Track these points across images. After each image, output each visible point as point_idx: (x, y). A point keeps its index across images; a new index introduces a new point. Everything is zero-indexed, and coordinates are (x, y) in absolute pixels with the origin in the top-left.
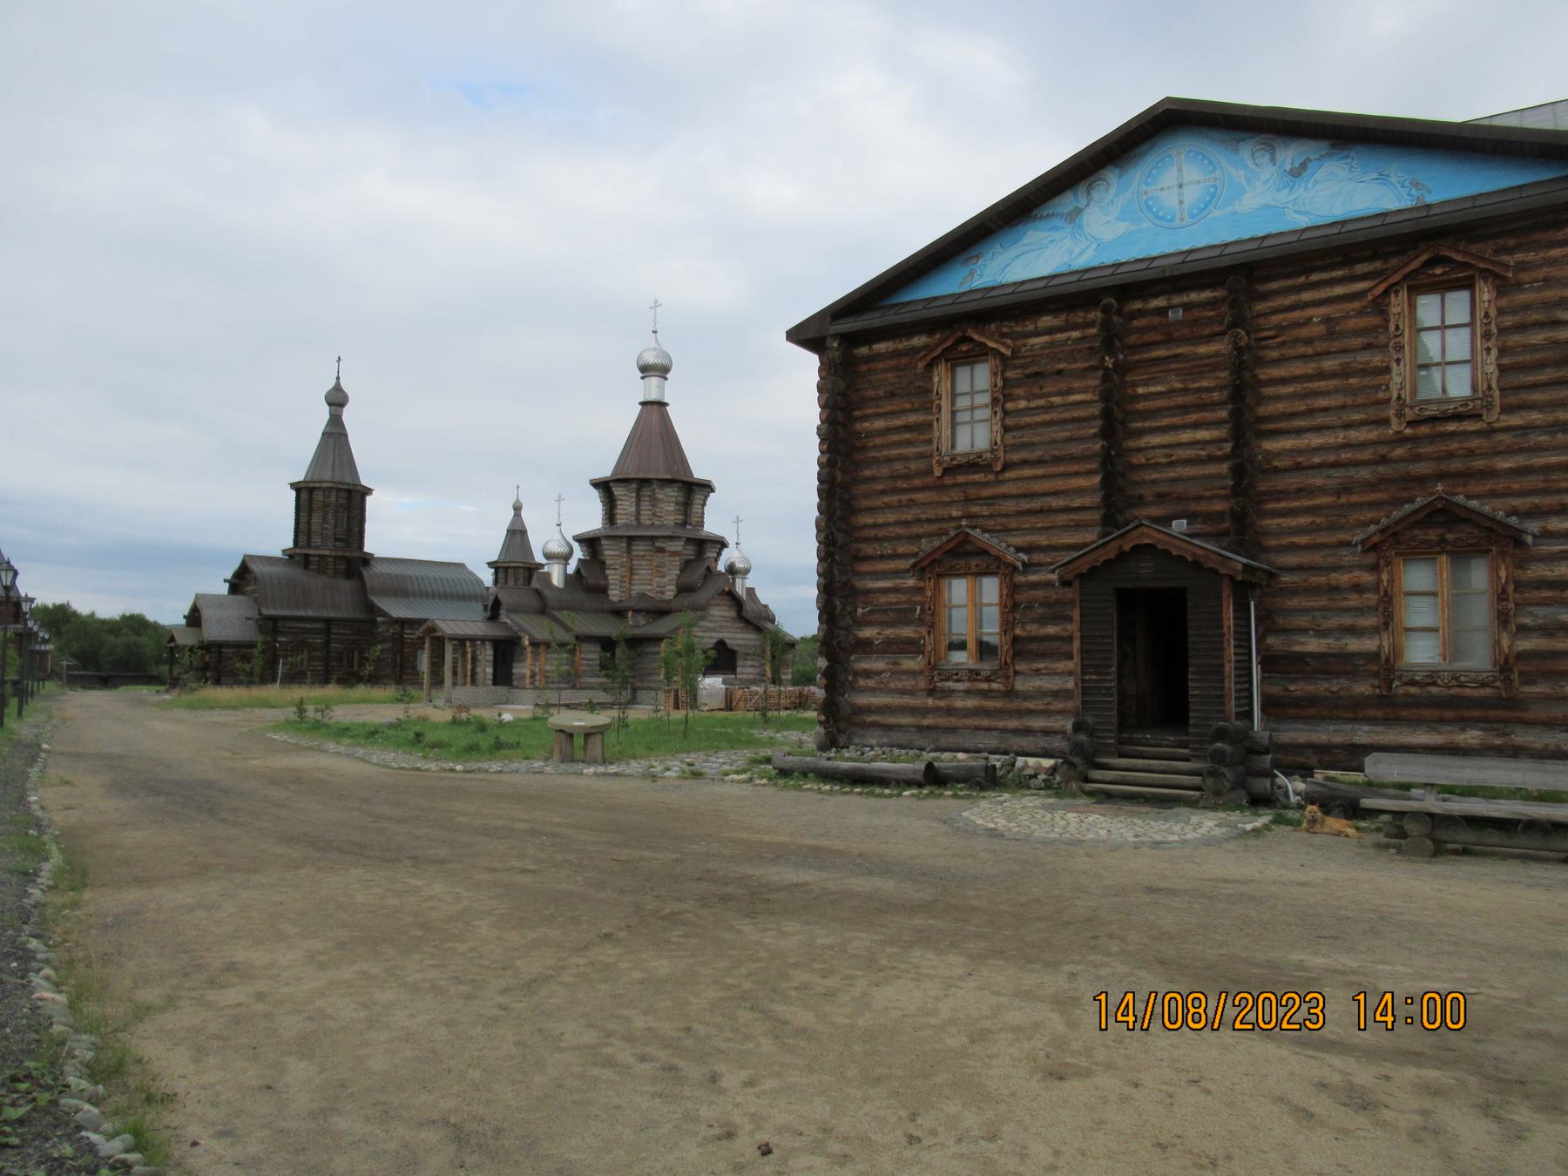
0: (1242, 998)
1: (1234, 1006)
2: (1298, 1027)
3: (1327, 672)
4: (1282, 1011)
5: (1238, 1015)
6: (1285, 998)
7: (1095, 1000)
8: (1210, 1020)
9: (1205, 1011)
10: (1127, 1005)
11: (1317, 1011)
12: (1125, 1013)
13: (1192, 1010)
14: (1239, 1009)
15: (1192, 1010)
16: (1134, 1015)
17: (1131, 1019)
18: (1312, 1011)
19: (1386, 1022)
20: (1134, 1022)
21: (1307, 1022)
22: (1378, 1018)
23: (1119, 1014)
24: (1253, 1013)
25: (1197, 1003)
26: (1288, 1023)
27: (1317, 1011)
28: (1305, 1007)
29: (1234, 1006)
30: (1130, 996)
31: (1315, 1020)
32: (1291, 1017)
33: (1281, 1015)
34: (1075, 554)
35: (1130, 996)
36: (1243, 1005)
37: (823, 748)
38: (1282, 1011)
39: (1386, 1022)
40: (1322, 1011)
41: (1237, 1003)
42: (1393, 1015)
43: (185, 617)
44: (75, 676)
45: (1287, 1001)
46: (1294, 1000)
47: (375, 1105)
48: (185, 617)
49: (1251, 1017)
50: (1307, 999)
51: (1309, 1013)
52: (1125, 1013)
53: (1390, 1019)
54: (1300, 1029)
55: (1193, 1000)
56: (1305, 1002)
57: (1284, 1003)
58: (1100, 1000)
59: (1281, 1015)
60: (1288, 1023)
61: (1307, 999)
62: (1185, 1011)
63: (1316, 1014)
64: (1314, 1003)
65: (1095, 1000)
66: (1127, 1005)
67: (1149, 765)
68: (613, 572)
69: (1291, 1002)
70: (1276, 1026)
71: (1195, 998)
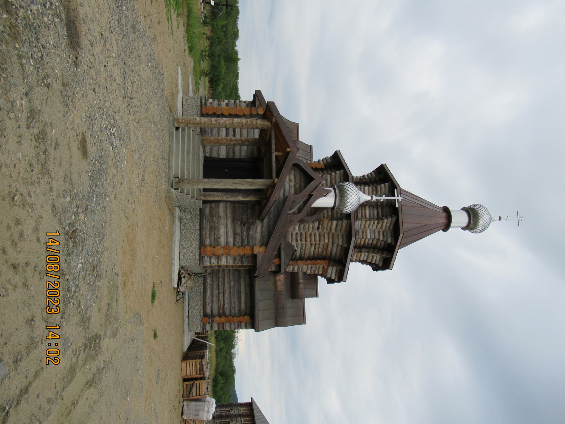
0: (57, 284)
1: (55, 281)
2: (47, 304)
3: (247, 296)
4: (53, 358)
5: (52, 283)
6: (58, 359)
7: (57, 231)
8: (49, 272)
9: (53, 313)
10: (55, 243)
11: (53, 311)
12: (52, 242)
13: (53, 269)
14: (54, 283)
15: (53, 266)
16: (51, 245)
17: (50, 244)
18: (53, 309)
19: (49, 243)
20: (49, 245)
21: (49, 308)
22: (50, 333)
23: (52, 240)
24: (53, 288)
25: (56, 268)
26: (49, 301)
27: (53, 311)
28: (54, 307)
29: (55, 281)
30: (58, 243)
31: (49, 310)
32: (50, 284)
33: (51, 357)
34: (417, 206)
35: (58, 243)
36: (55, 284)
37: (292, 181)
38: (53, 358)
39: (49, 243)
40: (53, 313)
41: (56, 282)
42: (51, 338)
43: (258, 95)
44: (195, 171)
45: (57, 309)
46: (57, 286)
47: (31, 165)
48: (258, 95)
49: (50, 287)
50: (57, 308)
51: (52, 308)
52: (52, 335)
53: (50, 337)
54: (46, 305)
55: (57, 266)
56: (56, 307)
57: (56, 299)
58: (57, 233)
59: (51, 357)
60: (49, 301)
61: (57, 308)
62: (53, 264)
63: (52, 311)
64: (56, 310)
65: (57, 231)
66: (55, 243)
67: (172, 161)
68: (316, 227)
69: (56, 285)
70: (48, 262)
71: (57, 267)
